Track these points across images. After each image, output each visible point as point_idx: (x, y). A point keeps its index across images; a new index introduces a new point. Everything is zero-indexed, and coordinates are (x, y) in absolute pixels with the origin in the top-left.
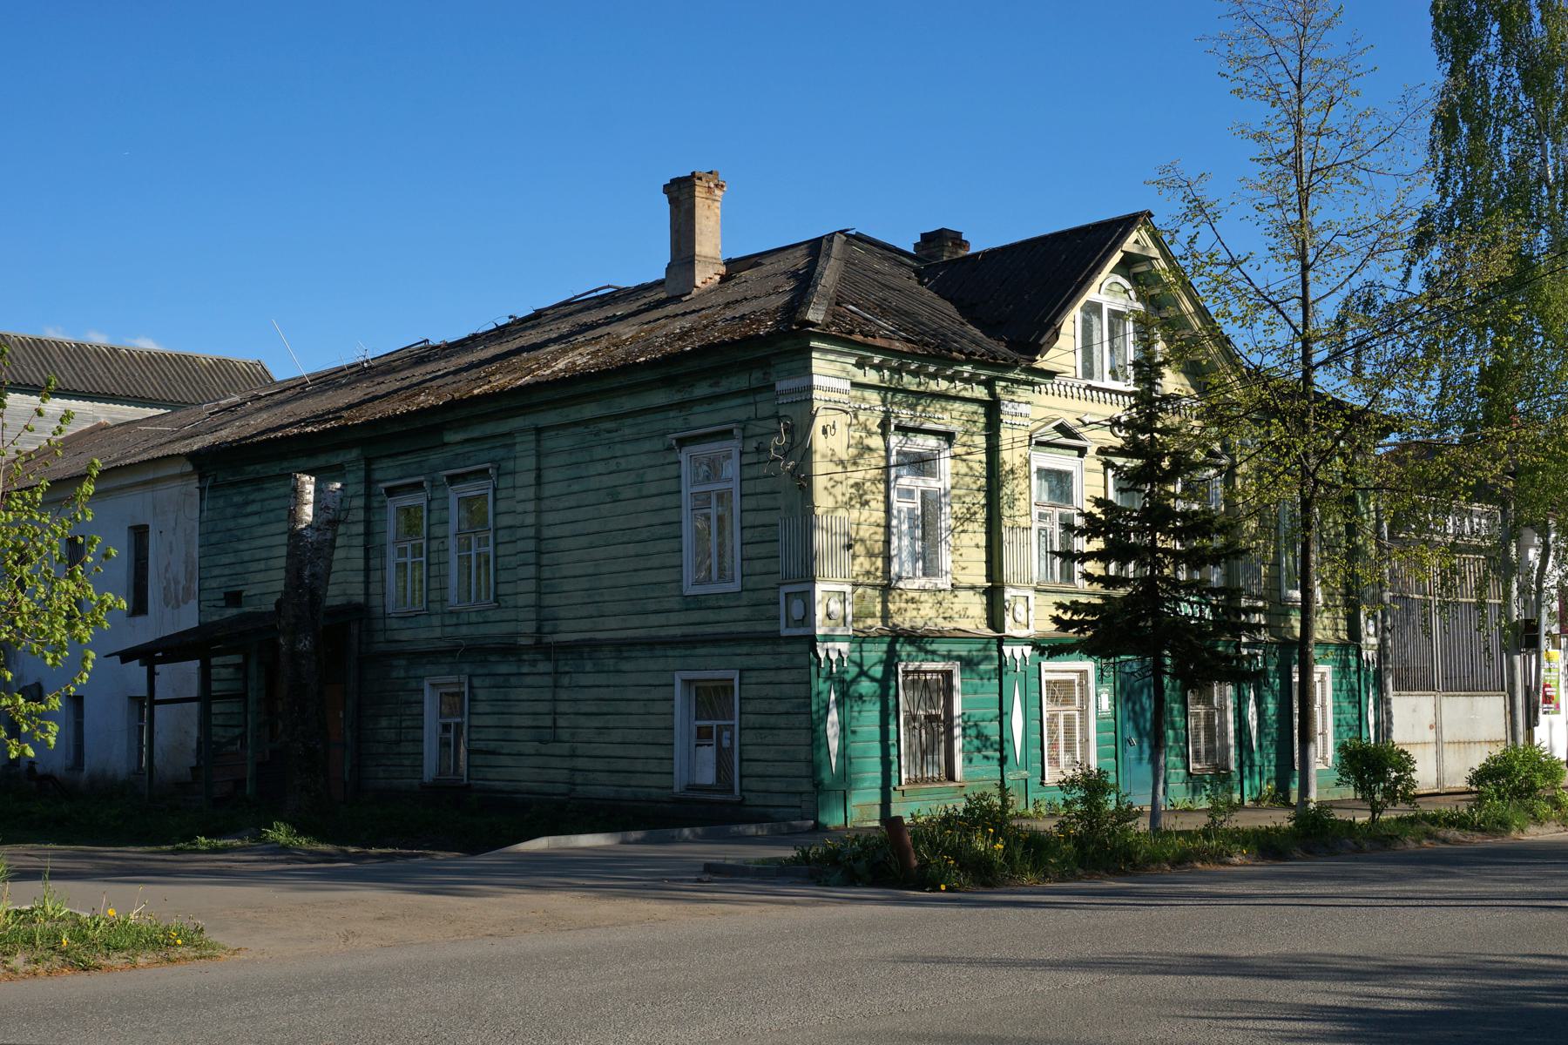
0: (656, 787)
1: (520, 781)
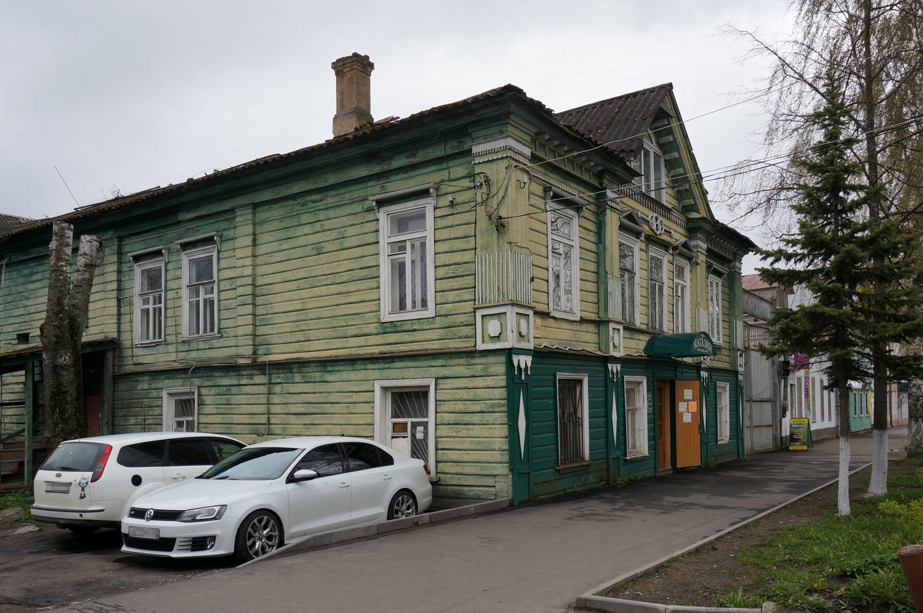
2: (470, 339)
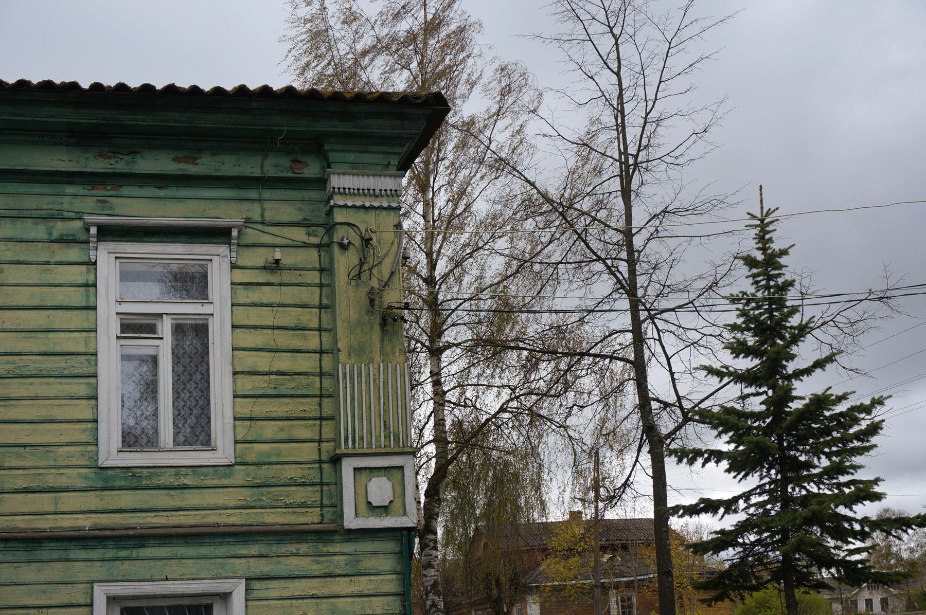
2: (312, 510)
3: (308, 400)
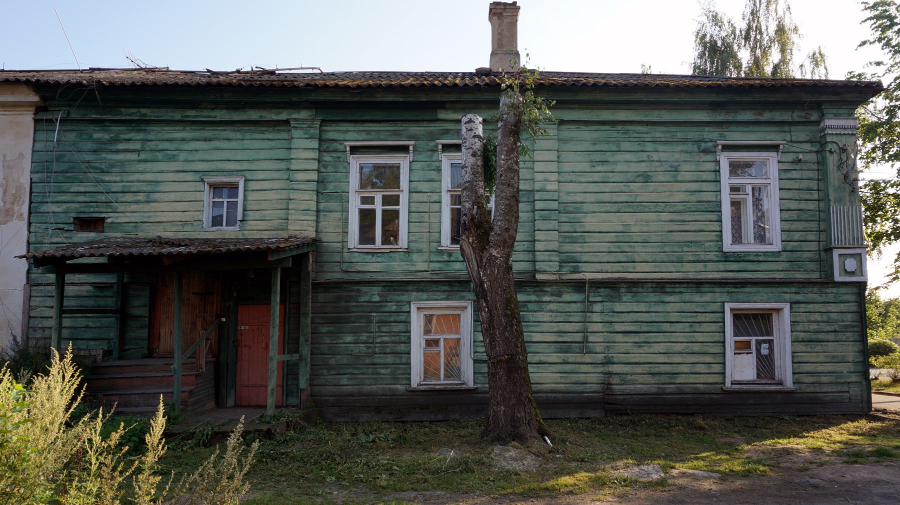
0: (704, 384)
1: (543, 384)
3: (814, 222)
